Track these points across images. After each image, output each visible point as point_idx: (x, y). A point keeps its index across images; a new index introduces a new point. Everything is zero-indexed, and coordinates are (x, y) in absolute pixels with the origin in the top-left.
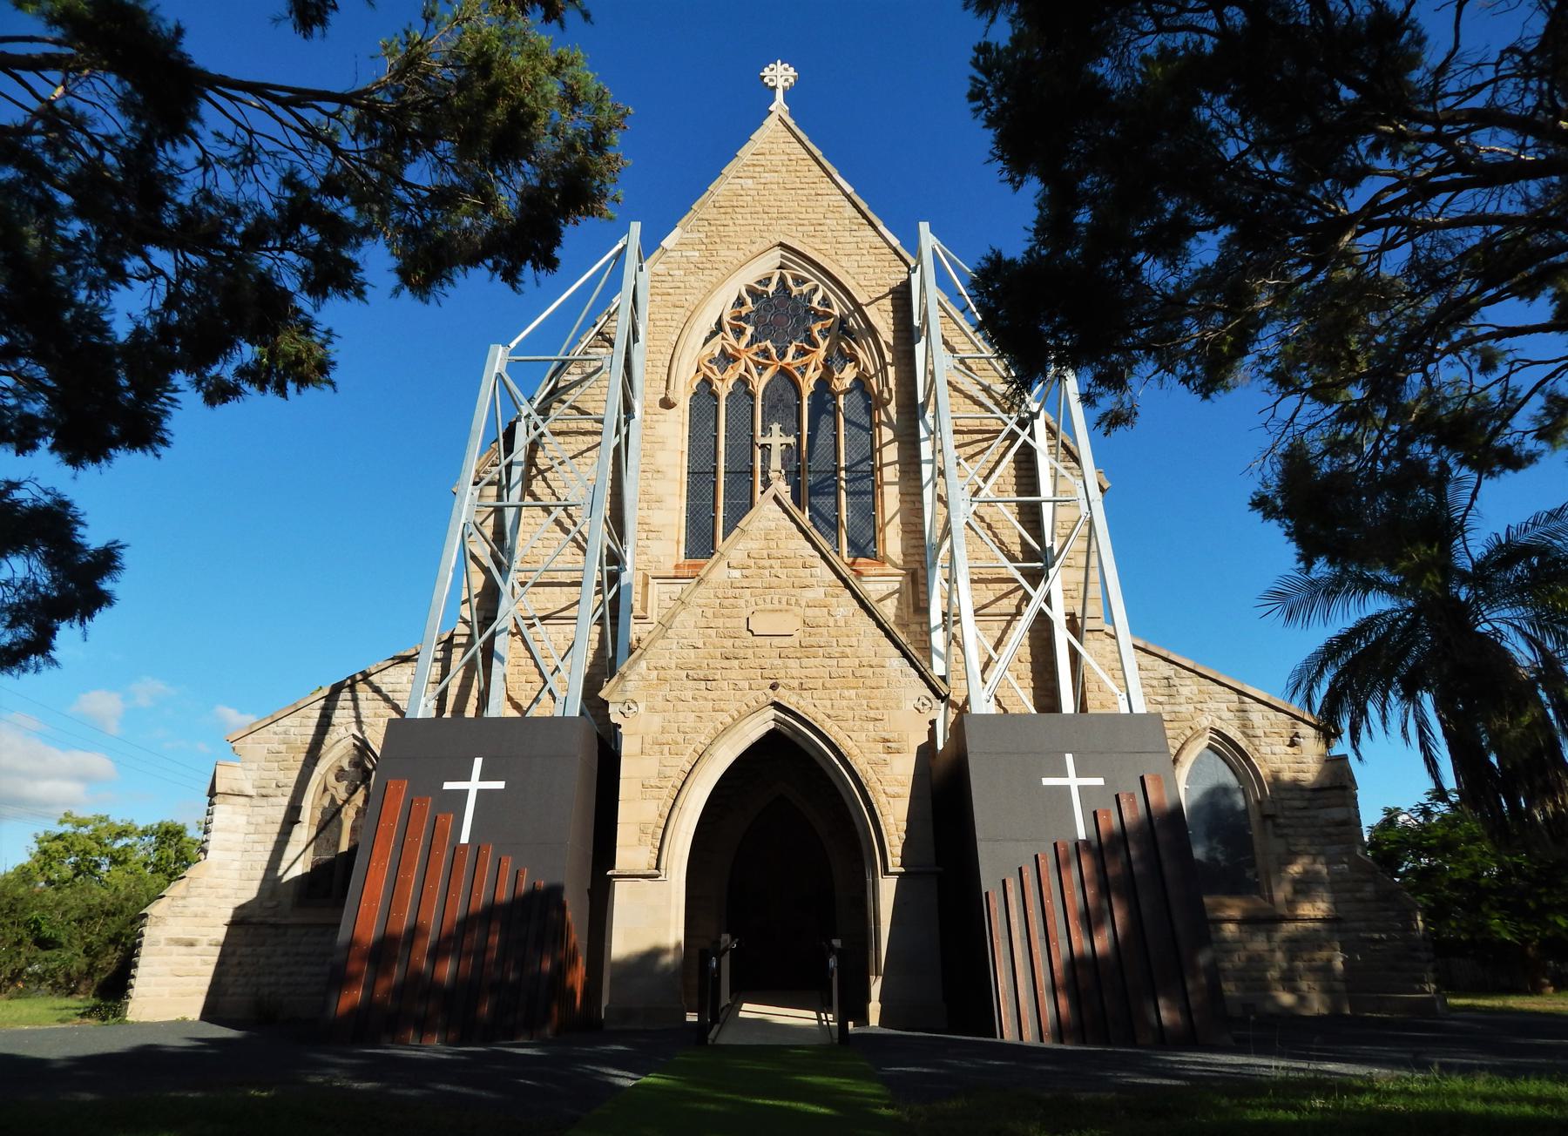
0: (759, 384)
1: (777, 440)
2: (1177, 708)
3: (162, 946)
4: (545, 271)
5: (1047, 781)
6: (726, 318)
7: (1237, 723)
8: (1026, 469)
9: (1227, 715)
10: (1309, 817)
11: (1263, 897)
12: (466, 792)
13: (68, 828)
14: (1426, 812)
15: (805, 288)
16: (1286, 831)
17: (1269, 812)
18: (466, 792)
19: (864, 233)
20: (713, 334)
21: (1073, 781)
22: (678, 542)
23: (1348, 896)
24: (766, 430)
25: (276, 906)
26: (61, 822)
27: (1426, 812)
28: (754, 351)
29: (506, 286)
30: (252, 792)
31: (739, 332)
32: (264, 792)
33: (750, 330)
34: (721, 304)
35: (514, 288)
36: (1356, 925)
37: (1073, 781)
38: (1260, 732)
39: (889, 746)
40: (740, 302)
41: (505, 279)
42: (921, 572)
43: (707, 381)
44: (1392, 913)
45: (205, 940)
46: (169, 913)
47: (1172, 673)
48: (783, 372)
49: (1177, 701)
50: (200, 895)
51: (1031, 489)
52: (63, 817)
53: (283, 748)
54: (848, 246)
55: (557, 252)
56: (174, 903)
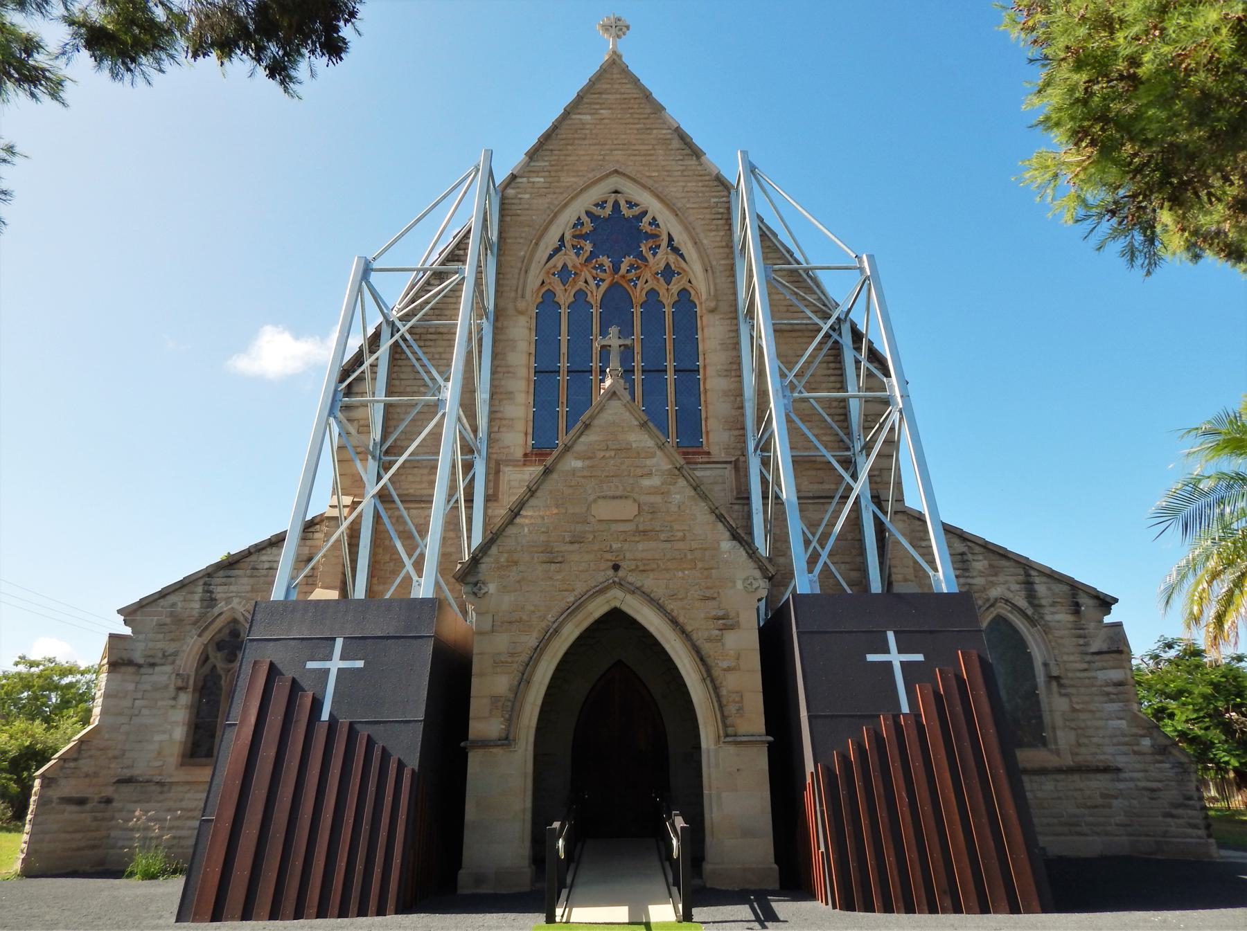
0: (596, 295)
1: (613, 339)
2: (970, 581)
3: (53, 805)
4: (325, 59)
5: (871, 658)
6: (568, 237)
7: (1023, 593)
8: (835, 369)
9: (1015, 587)
10: (1089, 678)
11: (1051, 751)
12: (342, 658)
13: (22, 668)
14: (1155, 657)
15: (636, 211)
16: (1069, 690)
17: (1055, 673)
18: (342, 658)
19: (690, 163)
20: (557, 250)
21: (896, 658)
22: (526, 434)
23: (1124, 748)
24: (604, 333)
25: (162, 766)
26: (16, 664)
27: (1155, 657)
28: (592, 265)
29: (273, 85)
30: (141, 661)
31: (578, 250)
32: (152, 661)
33: (588, 247)
34: (563, 225)
35: (286, 90)
36: (1135, 775)
37: (896, 658)
38: (1044, 602)
39: (727, 623)
40: (579, 223)
41: (272, 75)
42: (742, 459)
43: (550, 294)
44: (1167, 765)
45: (96, 797)
46: (61, 775)
47: (965, 549)
48: (614, 286)
49: (971, 574)
50: (91, 757)
51: (838, 385)
52: (18, 660)
53: (168, 620)
54: (676, 174)
55: (346, 31)
56: (67, 765)
